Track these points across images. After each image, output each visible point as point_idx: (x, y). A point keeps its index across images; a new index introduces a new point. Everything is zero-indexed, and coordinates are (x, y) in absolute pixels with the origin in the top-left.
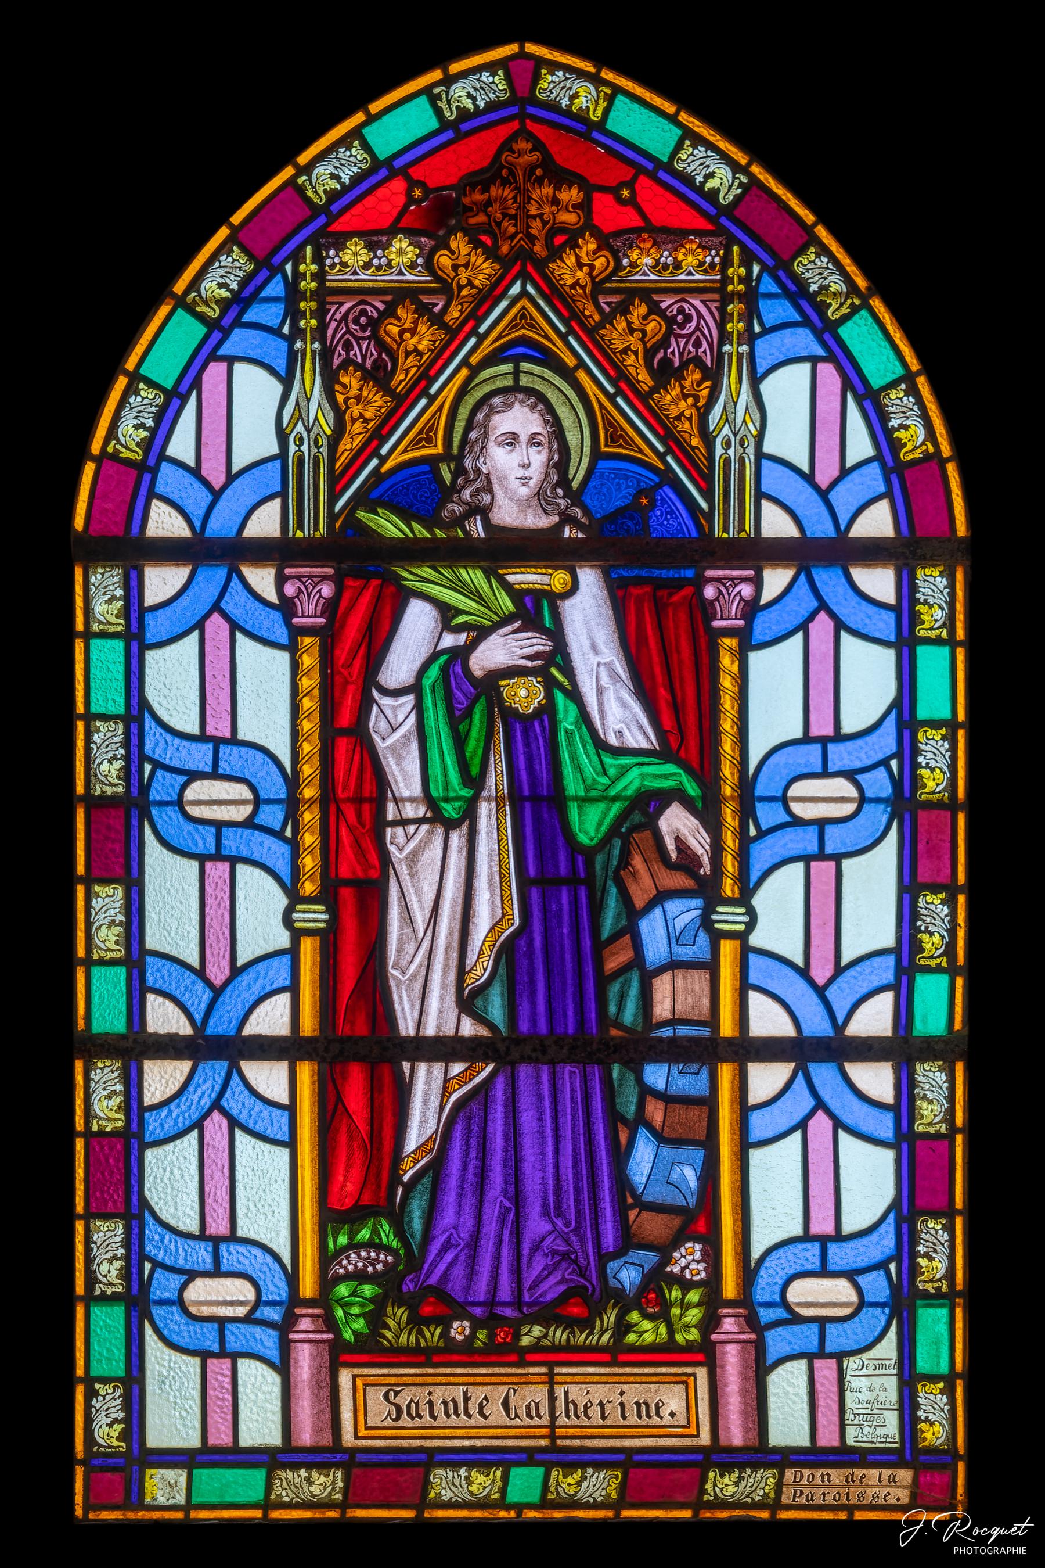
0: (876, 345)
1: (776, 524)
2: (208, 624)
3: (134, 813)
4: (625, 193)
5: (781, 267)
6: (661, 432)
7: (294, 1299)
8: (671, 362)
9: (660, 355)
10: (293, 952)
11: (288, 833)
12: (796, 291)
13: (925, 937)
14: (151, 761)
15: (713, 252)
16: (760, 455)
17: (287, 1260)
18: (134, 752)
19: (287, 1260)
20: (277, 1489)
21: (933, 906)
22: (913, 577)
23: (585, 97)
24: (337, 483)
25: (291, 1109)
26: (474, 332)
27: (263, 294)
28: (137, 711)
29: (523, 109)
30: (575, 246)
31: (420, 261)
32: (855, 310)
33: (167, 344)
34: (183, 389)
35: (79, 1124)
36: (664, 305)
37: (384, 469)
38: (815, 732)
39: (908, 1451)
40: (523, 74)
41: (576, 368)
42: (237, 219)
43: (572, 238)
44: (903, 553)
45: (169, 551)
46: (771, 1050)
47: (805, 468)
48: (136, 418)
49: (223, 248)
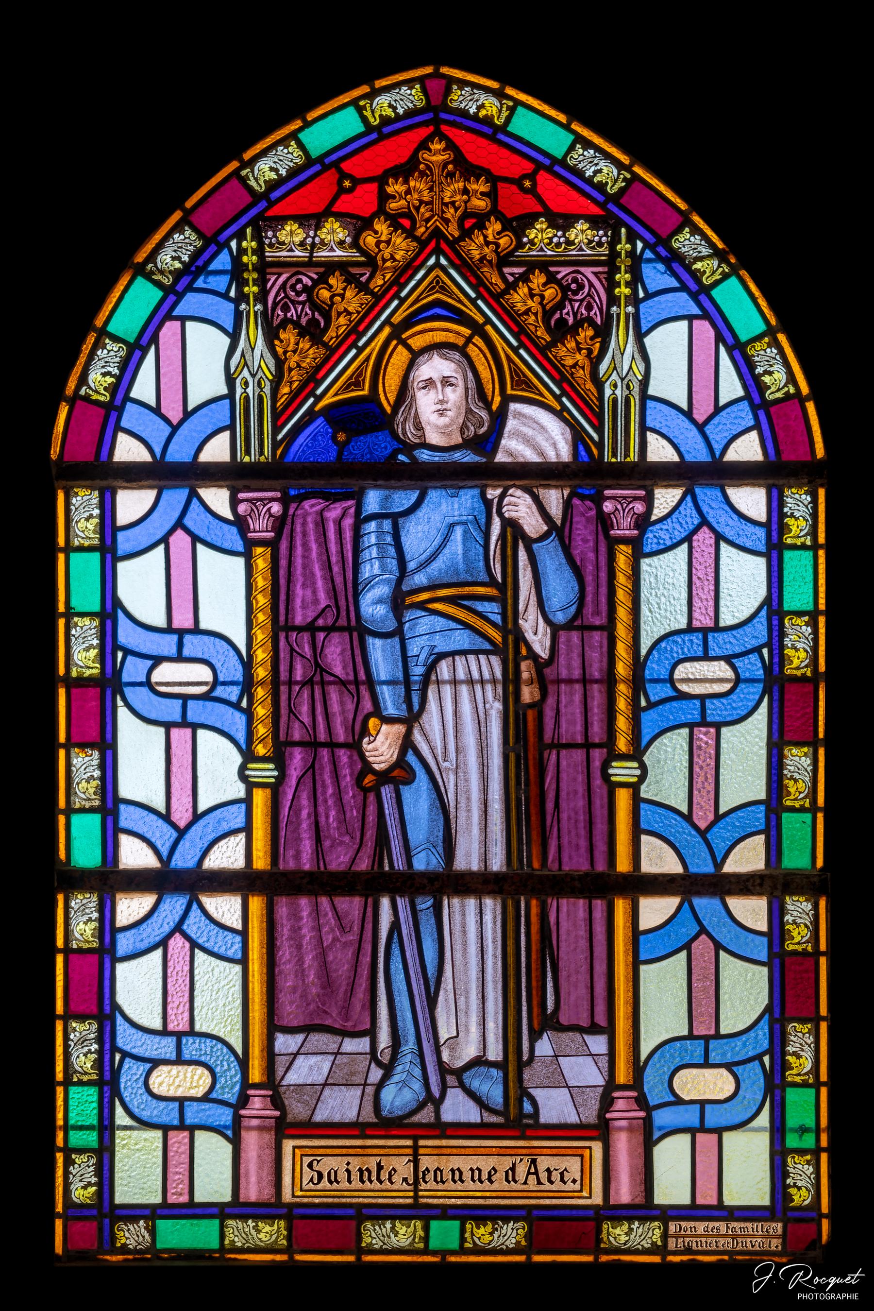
0: (742, 305)
1: (660, 451)
4: (527, 184)
7: (246, 1084)
8: (566, 321)
9: (557, 316)
10: (248, 801)
11: (244, 704)
12: (674, 261)
13: (625, 1227)
14: (120, 1051)
15: (601, 233)
16: (645, 397)
17: (239, 1051)
18: (109, 645)
19: (239, 1051)
21: (798, 760)
23: (491, 106)
25: (244, 934)
26: (396, 296)
27: (212, 267)
28: (111, 610)
30: (482, 227)
31: (349, 240)
32: (725, 277)
33: (132, 305)
34: (144, 341)
35: (60, 943)
36: (559, 276)
37: (317, 408)
40: (437, 92)
41: (485, 324)
43: (480, 220)
46: (660, 885)
47: (684, 406)
49: (178, 228)
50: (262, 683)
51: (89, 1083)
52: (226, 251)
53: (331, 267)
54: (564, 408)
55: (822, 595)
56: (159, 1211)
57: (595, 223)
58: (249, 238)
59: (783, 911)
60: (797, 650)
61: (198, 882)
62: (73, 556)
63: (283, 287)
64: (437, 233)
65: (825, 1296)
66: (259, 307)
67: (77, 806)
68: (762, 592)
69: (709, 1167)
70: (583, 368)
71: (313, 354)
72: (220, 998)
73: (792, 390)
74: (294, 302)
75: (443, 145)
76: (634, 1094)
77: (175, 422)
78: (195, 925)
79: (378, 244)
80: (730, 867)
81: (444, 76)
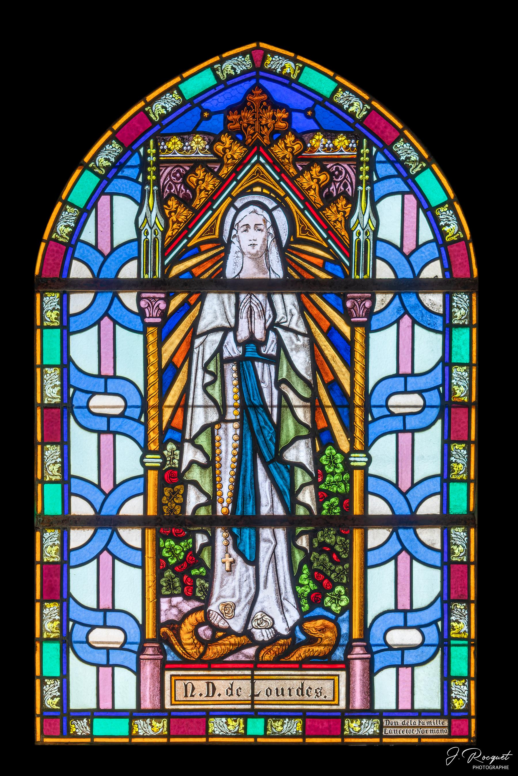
0: (434, 186)
1: (384, 272)
2: (102, 322)
3: (66, 411)
5: (387, 147)
6: (326, 227)
7: (143, 640)
9: (327, 190)
10: (145, 476)
11: (142, 420)
13: (455, 547)
14: (72, 620)
15: (353, 141)
16: (376, 239)
17: (142, 388)
20: (135, 730)
22: (449, 533)
23: (289, 67)
24: (165, 252)
25: (143, 550)
27: (129, 164)
28: (66, 363)
29: (257, 73)
30: (283, 138)
31: (207, 147)
32: (423, 169)
33: (81, 186)
35: (38, 558)
36: (328, 167)
37: (189, 245)
39: (446, 711)
42: (116, 126)
43: (282, 135)
44: (446, 286)
46: (380, 522)
48: (65, 222)
49: (108, 141)
52: (137, 154)
53: (196, 164)
54: (330, 246)
55: (474, 354)
56: (95, 714)
57: (349, 135)
58: (151, 147)
59: (451, 300)
60: (459, 386)
62: (45, 331)
63: (169, 174)
65: (489, 767)
67: (48, 479)
68: (439, 354)
70: (341, 222)
71: (184, 214)
72: (129, 588)
74: (175, 184)
76: (365, 644)
77: (105, 552)
78: (115, 546)
81: (262, 49)
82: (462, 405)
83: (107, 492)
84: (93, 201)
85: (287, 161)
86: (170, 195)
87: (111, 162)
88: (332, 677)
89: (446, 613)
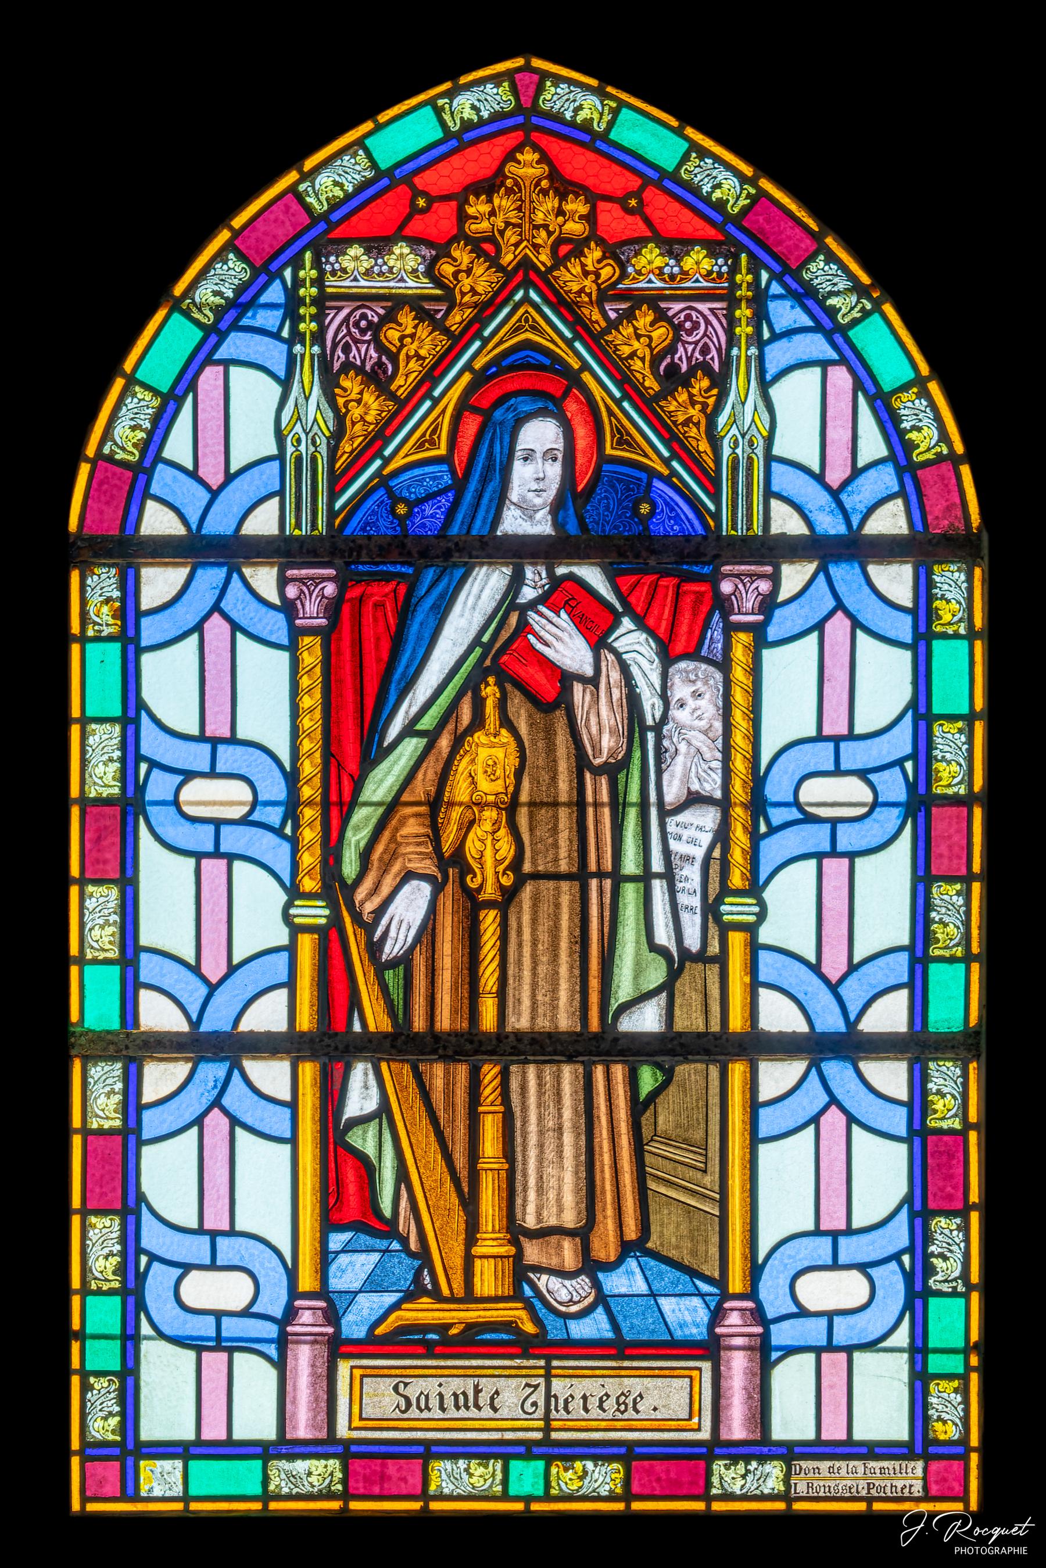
0: (887, 346)
1: (786, 522)
7: (294, 1293)
9: (668, 360)
10: (292, 949)
11: (288, 830)
12: (806, 295)
15: (720, 261)
16: (770, 458)
18: (130, 754)
22: (930, 573)
24: (337, 482)
25: (293, 1105)
27: (263, 299)
28: (133, 710)
32: (866, 314)
33: (164, 346)
34: (179, 391)
35: (76, 1122)
36: (670, 313)
38: (827, 731)
39: (920, 1445)
40: (527, 90)
43: (577, 247)
45: (164, 550)
46: (784, 1046)
49: (220, 256)
50: (310, 803)
51: (111, 1292)
53: (396, 303)
54: (674, 473)
57: (713, 249)
59: (925, 1078)
61: (233, 1048)
64: (525, 264)
66: (316, 349)
68: (904, 693)
69: (837, 1394)
70: (697, 425)
72: (269, 1187)
73: (945, 451)
74: (356, 342)
75: (536, 156)
79: (455, 275)
80: (869, 1024)
82: (955, 801)
83: (215, 488)
84: (189, 376)
85: (587, 299)
86: (347, 367)
87: (226, 299)
88: (686, 1372)
89: (921, 1238)
